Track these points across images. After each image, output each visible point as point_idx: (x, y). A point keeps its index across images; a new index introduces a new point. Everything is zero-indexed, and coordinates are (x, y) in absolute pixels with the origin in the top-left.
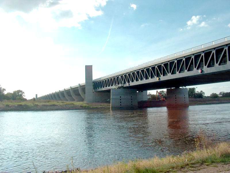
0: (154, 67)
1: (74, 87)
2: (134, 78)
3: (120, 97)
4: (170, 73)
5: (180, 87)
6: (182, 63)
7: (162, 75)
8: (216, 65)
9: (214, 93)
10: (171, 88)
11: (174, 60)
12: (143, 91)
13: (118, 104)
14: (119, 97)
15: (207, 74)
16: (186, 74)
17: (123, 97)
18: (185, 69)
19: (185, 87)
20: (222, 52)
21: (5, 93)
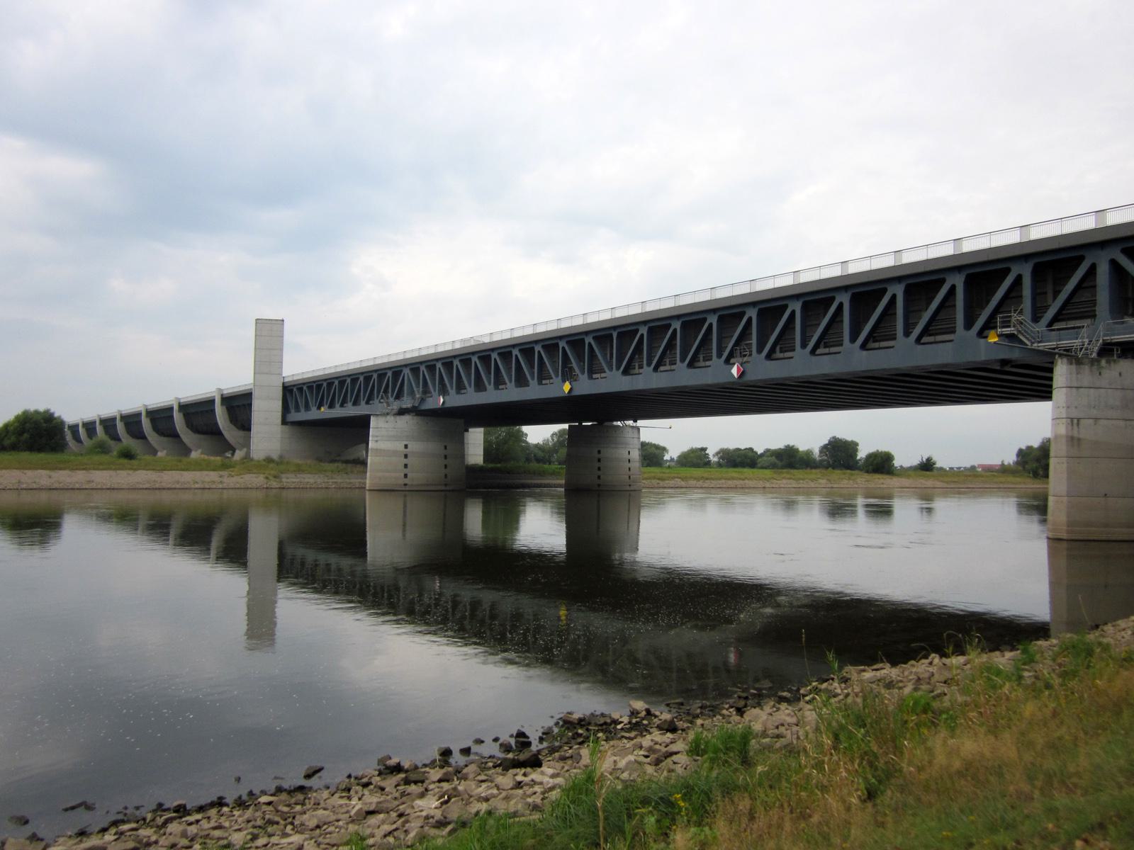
0: (449, 362)
1: (184, 404)
2: (365, 392)
3: (406, 446)
4: (618, 368)
5: (615, 423)
6: (668, 336)
7: (557, 376)
8: (681, 367)
9: (788, 445)
10: (580, 424)
11: (385, 369)
12: (470, 430)
13: (395, 478)
14: (399, 446)
15: (787, 382)
16: (647, 379)
17: (415, 446)
18: (645, 362)
19: (635, 421)
20: (937, 291)
21: (759, 453)
